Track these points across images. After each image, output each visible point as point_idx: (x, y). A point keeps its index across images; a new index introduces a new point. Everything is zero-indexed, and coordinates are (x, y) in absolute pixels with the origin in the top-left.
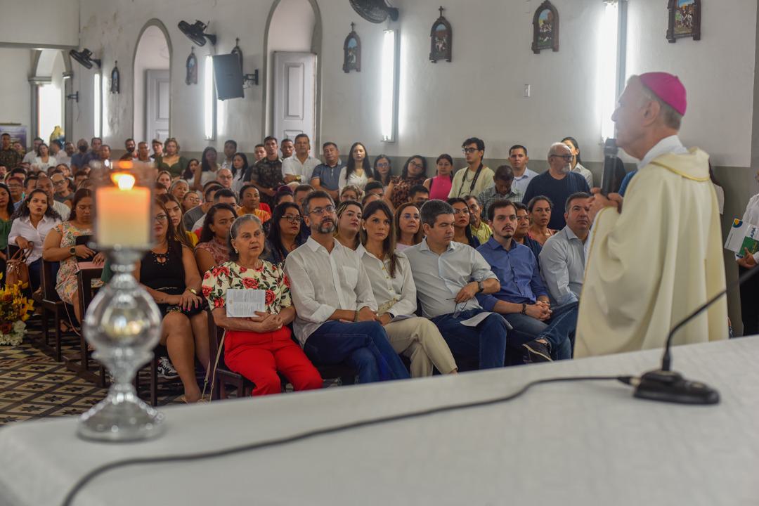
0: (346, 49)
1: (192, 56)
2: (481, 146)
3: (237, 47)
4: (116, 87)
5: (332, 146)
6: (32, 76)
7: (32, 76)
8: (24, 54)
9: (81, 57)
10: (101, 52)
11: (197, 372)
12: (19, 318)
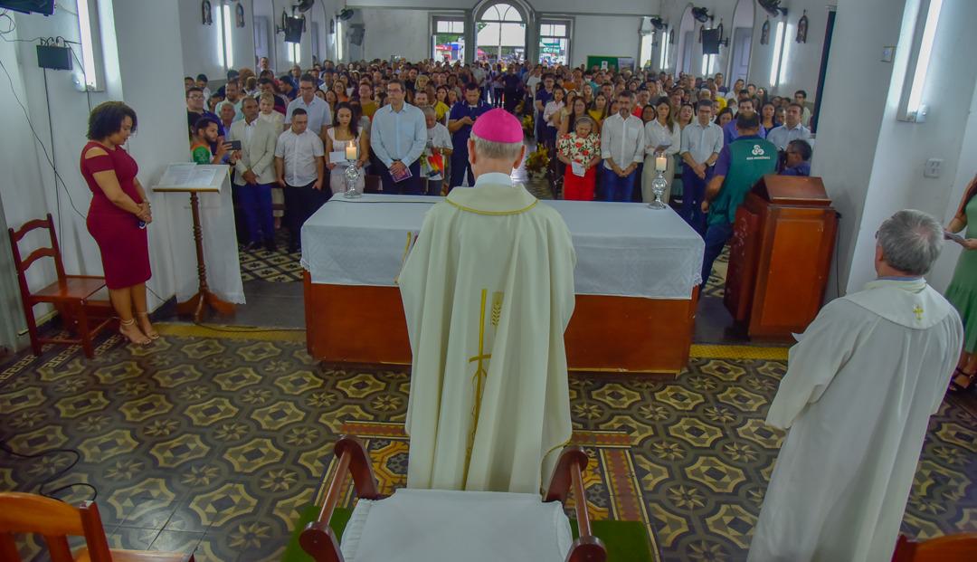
0: (764, 30)
1: (767, 23)
2: (805, 96)
3: (805, 17)
4: (672, 42)
5: (752, 87)
6: (640, 30)
7: (640, 30)
8: (637, 20)
9: (658, 23)
10: (668, 20)
11: (518, 108)
12: (544, 165)
